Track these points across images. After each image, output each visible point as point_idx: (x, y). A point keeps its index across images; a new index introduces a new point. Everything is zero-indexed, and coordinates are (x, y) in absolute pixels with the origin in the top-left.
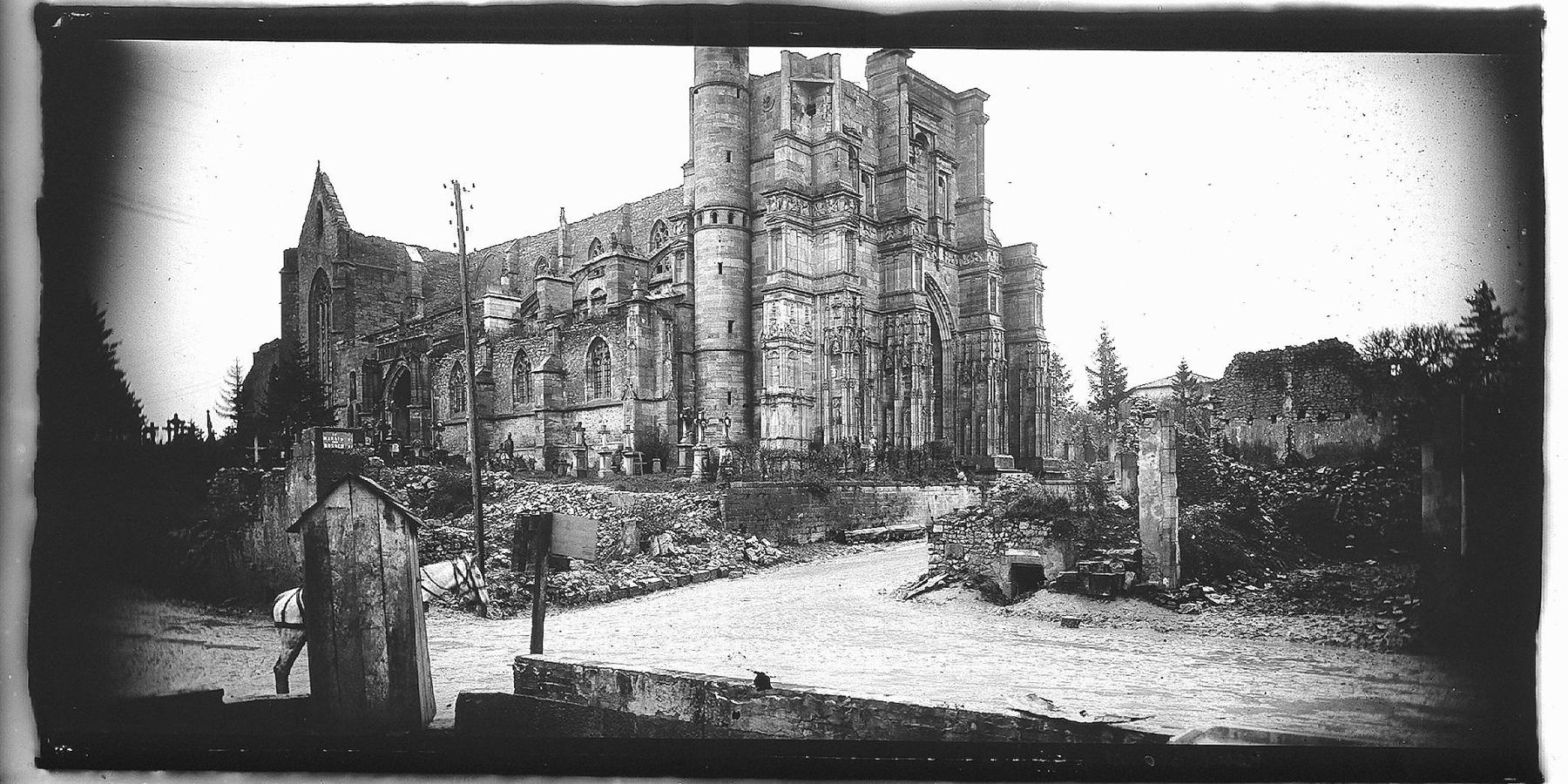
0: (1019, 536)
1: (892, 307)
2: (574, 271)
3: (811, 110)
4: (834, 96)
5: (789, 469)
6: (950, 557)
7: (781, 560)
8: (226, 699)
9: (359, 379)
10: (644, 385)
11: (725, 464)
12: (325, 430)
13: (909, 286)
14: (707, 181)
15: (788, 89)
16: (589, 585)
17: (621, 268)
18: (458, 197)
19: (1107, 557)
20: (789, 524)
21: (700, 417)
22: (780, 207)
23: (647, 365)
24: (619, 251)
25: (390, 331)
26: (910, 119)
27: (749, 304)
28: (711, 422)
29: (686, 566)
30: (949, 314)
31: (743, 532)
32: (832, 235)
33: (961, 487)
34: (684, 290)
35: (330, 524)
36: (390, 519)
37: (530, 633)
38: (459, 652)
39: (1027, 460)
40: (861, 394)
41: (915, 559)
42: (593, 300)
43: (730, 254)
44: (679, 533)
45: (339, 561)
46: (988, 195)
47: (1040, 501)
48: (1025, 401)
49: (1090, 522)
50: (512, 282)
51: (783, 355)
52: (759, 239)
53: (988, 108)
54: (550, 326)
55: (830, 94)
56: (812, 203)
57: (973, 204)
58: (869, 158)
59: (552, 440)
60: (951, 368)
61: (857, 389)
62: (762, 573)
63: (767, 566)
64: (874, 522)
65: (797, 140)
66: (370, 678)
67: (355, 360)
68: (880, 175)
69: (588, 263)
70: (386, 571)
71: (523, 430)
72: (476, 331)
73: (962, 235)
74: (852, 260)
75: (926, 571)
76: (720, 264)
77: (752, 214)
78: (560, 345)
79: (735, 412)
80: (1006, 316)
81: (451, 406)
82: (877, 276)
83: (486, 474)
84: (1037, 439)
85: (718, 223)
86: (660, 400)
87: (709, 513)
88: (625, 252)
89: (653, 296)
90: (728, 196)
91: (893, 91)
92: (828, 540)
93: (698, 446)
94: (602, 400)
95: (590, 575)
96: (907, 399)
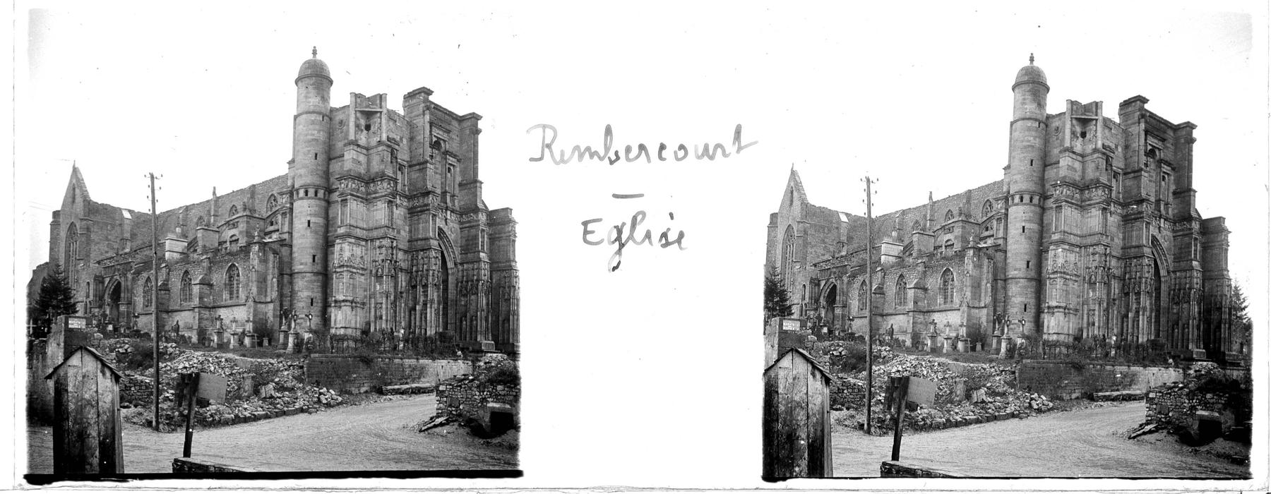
0: (496, 395)
1: (416, 248)
2: (936, 229)
3: (1083, 135)
4: (383, 120)
5: (1060, 353)
6: (450, 406)
7: (1052, 409)
9: (92, 287)
11: (1020, 348)
12: (70, 317)
13: (428, 235)
14: (1018, 177)
15: (1070, 122)
17: (248, 222)
18: (869, 187)
20: (347, 381)
21: (293, 313)
22: (347, 186)
23: (262, 281)
24: (963, 218)
25: (110, 258)
27: (1040, 253)
28: (300, 316)
29: (993, 410)
30: (1166, 260)
31: (1030, 390)
33: (459, 361)
34: (286, 236)
35: (779, 377)
36: (103, 373)
37: (892, 446)
38: (143, 452)
41: (1138, 413)
42: (946, 246)
43: (1030, 221)
44: (278, 384)
45: (783, 399)
46: (480, 178)
47: (1221, 381)
48: (1215, 316)
50: (182, 230)
51: (1060, 282)
52: (1048, 212)
53: (1195, 133)
54: (920, 261)
55: (1096, 125)
56: (367, 183)
57: (471, 184)
58: (1118, 164)
59: (202, 325)
60: (1166, 293)
61: (1105, 304)
64: (1113, 388)
65: (1074, 153)
66: (88, 467)
67: (806, 277)
68: (1125, 174)
70: (100, 404)
72: (159, 259)
73: (462, 203)
74: (391, 218)
75: (1144, 422)
76: (1024, 227)
77: (1044, 197)
78: (210, 268)
80: (491, 253)
83: (162, 345)
84: (1222, 340)
85: (309, 196)
86: (269, 302)
87: (1009, 378)
88: (966, 219)
89: (982, 245)
90: (1030, 186)
91: (419, 115)
92: (371, 391)
93: (1005, 336)
94: (948, 306)
96: (425, 304)
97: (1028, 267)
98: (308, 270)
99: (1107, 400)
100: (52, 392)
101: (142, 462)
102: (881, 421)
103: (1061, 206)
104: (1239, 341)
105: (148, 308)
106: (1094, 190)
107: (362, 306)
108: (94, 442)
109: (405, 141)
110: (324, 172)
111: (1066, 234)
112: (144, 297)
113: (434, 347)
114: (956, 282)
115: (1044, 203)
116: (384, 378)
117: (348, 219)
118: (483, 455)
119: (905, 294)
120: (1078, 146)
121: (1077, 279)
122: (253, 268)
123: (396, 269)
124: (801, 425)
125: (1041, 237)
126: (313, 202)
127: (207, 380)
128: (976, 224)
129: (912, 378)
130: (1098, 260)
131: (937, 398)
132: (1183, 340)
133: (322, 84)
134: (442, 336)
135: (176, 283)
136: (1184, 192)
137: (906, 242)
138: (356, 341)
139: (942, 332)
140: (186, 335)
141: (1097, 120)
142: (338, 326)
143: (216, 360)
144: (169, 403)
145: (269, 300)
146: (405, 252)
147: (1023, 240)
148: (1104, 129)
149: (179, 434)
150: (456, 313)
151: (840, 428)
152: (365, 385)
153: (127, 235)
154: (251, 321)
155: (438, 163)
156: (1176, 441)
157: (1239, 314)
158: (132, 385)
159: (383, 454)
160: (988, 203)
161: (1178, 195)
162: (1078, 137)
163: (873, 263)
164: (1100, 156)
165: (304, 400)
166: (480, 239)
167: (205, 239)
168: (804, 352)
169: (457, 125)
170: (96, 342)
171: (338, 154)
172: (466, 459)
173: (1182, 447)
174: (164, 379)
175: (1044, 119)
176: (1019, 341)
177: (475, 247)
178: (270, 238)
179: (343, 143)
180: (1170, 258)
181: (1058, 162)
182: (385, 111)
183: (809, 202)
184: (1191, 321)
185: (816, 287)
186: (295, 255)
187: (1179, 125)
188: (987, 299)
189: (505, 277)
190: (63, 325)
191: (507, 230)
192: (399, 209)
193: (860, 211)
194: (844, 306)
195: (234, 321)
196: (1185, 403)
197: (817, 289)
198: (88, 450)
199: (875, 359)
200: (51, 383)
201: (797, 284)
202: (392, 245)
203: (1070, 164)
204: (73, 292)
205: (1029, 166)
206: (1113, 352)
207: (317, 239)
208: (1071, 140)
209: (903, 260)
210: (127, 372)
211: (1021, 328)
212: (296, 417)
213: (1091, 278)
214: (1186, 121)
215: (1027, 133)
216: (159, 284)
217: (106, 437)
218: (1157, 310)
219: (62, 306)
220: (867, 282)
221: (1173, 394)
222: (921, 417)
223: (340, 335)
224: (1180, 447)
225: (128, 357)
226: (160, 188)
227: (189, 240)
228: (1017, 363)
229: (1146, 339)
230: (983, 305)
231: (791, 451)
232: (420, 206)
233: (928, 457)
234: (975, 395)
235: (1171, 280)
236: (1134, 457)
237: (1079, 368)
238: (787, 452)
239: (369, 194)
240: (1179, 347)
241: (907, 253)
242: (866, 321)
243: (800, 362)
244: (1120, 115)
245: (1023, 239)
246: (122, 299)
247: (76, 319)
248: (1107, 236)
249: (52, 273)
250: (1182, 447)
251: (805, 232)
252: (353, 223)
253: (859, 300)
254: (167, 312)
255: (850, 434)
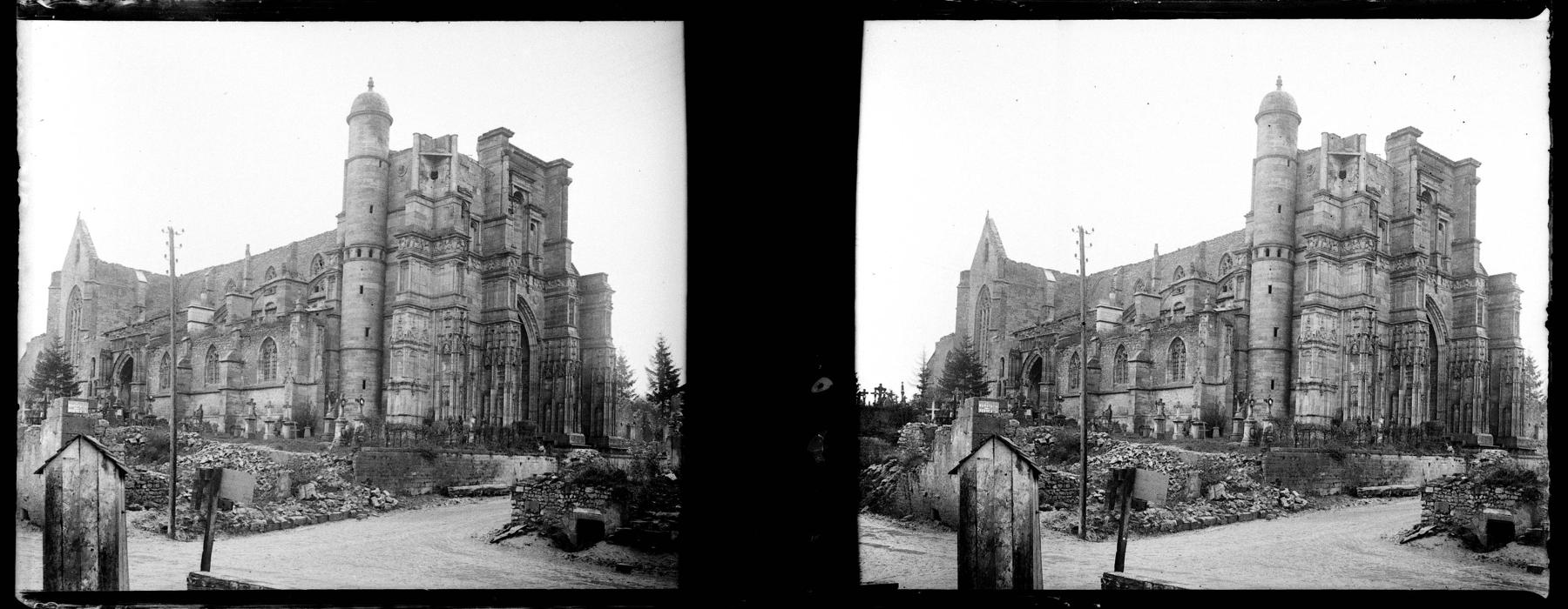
1: (491, 321)
3: (434, 176)
4: (1361, 166)
5: (407, 438)
6: (1438, 512)
8: (900, 588)
10: (1209, 373)
12: (980, 399)
16: (252, 519)
17: (1196, 287)
19: (656, 518)
20: (1314, 480)
23: (1213, 358)
26: (1418, 181)
28: (349, 401)
29: (325, 509)
32: (446, 266)
37: (1115, 553)
39: (596, 439)
40: (1373, 384)
41: (501, 511)
42: (1175, 311)
44: (321, 483)
45: (983, 496)
46: (570, 237)
48: (596, 393)
49: (643, 490)
50: (1117, 295)
51: (406, 353)
53: (1479, 173)
54: (235, 329)
55: (450, 164)
56: (1341, 241)
57: (558, 243)
59: (231, 411)
60: (536, 366)
61: (461, 380)
62: (383, 516)
63: (387, 511)
65: (423, 197)
66: (999, 582)
69: (264, 284)
71: (1120, 404)
73: (548, 266)
74: (1370, 286)
75: (510, 522)
76: (1270, 287)
77: (1295, 250)
78: (1150, 342)
79: (1277, 394)
80: (1490, 327)
81: (160, 384)
82: (480, 297)
85: (362, 256)
87: (1253, 469)
88: (292, 279)
91: (1405, 160)
92: (434, 493)
93: (339, 419)
94: (269, 383)
95: (1162, 511)
96: (1409, 388)
97: (367, 335)
98: (1268, 346)
99: (464, 496)
100: (957, 490)
101: (1065, 577)
102: (189, 523)
103: (407, 261)
104: (625, 423)
105: (1075, 390)
106: (447, 241)
107: (1333, 390)
108: (1007, 552)
109: (1387, 192)
110: (1289, 227)
111: (1322, 295)
112: (1070, 376)
113: (1419, 441)
114: (1188, 354)
115: (386, 258)
116: (1358, 477)
117: (1318, 285)
118: (1477, 572)
119: (1126, 368)
120: (428, 188)
121: (427, 349)
122: (1202, 342)
123: (1375, 345)
124: (1005, 528)
125: (383, 299)
126: (1276, 263)
127: (1144, 478)
128: (1212, 283)
129: (1139, 470)
130: (452, 326)
131: (257, 494)
132: (556, 422)
133: (1288, 122)
134: (521, 427)
135: (200, 362)
136: (558, 243)
137: (218, 307)
138: (1325, 432)
139: (262, 414)
140: (1120, 423)
141: (450, 157)
142: (1304, 413)
143: (1156, 454)
144: (1099, 505)
145: (312, 381)
146: (1386, 325)
147: (361, 303)
148: (459, 170)
149: (1109, 544)
150: (1447, 400)
151: (137, 532)
152: (427, 485)
153: (1050, 302)
154: (290, 407)
155: (519, 218)
156: (549, 545)
157: (625, 391)
158: (1054, 483)
159: (1356, 570)
160: (318, 259)
161: (550, 248)
162: (427, 179)
163: (178, 331)
164: (455, 200)
165: (1261, 503)
166: (1477, 311)
167: (1145, 308)
168: (94, 440)
169: (1450, 173)
170: (1011, 431)
171: (399, 206)
172: (1457, 578)
173: (556, 553)
174: (1093, 475)
175: (386, 157)
176: (1265, 425)
177: (1471, 321)
178: (1223, 306)
179: (1312, 193)
180: (541, 324)
181: (404, 209)
182: (1363, 155)
183: (99, 257)
184: (1474, 400)
185: (1018, 361)
186: (1252, 328)
187: (551, 163)
188: (316, 374)
189: (1507, 357)
190: (61, 409)
191: (1509, 300)
192: (1379, 272)
193: (161, 268)
194: (143, 384)
195: (1179, 406)
196: (560, 498)
197: (109, 365)
198: (86, 561)
199: (181, 447)
200: (956, 479)
201: (993, 357)
202: (1370, 317)
203: (418, 210)
204: (75, 370)
205: (1276, 214)
206: (472, 438)
207: (1279, 308)
208: (1328, 181)
209: (215, 328)
210: (1048, 467)
211: (1268, 409)
212: (1252, 524)
213: (1352, 348)
214: (559, 158)
215: (365, 174)
216: (1088, 361)
217: (1021, 546)
218: (525, 386)
219: (970, 386)
220: (171, 355)
221: (545, 487)
222: (237, 517)
223: (1306, 424)
224: (1463, 554)
225: (1049, 449)
226: (1091, 245)
227: (1125, 308)
228: (1264, 451)
229: (512, 421)
230: (1221, 382)
231: (78, 560)
232: (497, 271)
233: (245, 567)
234: (303, 490)
235: (542, 350)
236: (497, 565)
237: (430, 457)
238: (73, 561)
239: (1342, 254)
240: (1460, 431)
241: (219, 320)
242: (169, 402)
243: (88, 451)
244: (1387, 151)
245: (361, 302)
246: (134, 378)
247: (77, 403)
248: (464, 297)
249: (50, 348)
250: (556, 553)
251: (94, 294)
252: (415, 289)
253: (161, 376)
254: (1098, 395)
255: (1061, 540)
